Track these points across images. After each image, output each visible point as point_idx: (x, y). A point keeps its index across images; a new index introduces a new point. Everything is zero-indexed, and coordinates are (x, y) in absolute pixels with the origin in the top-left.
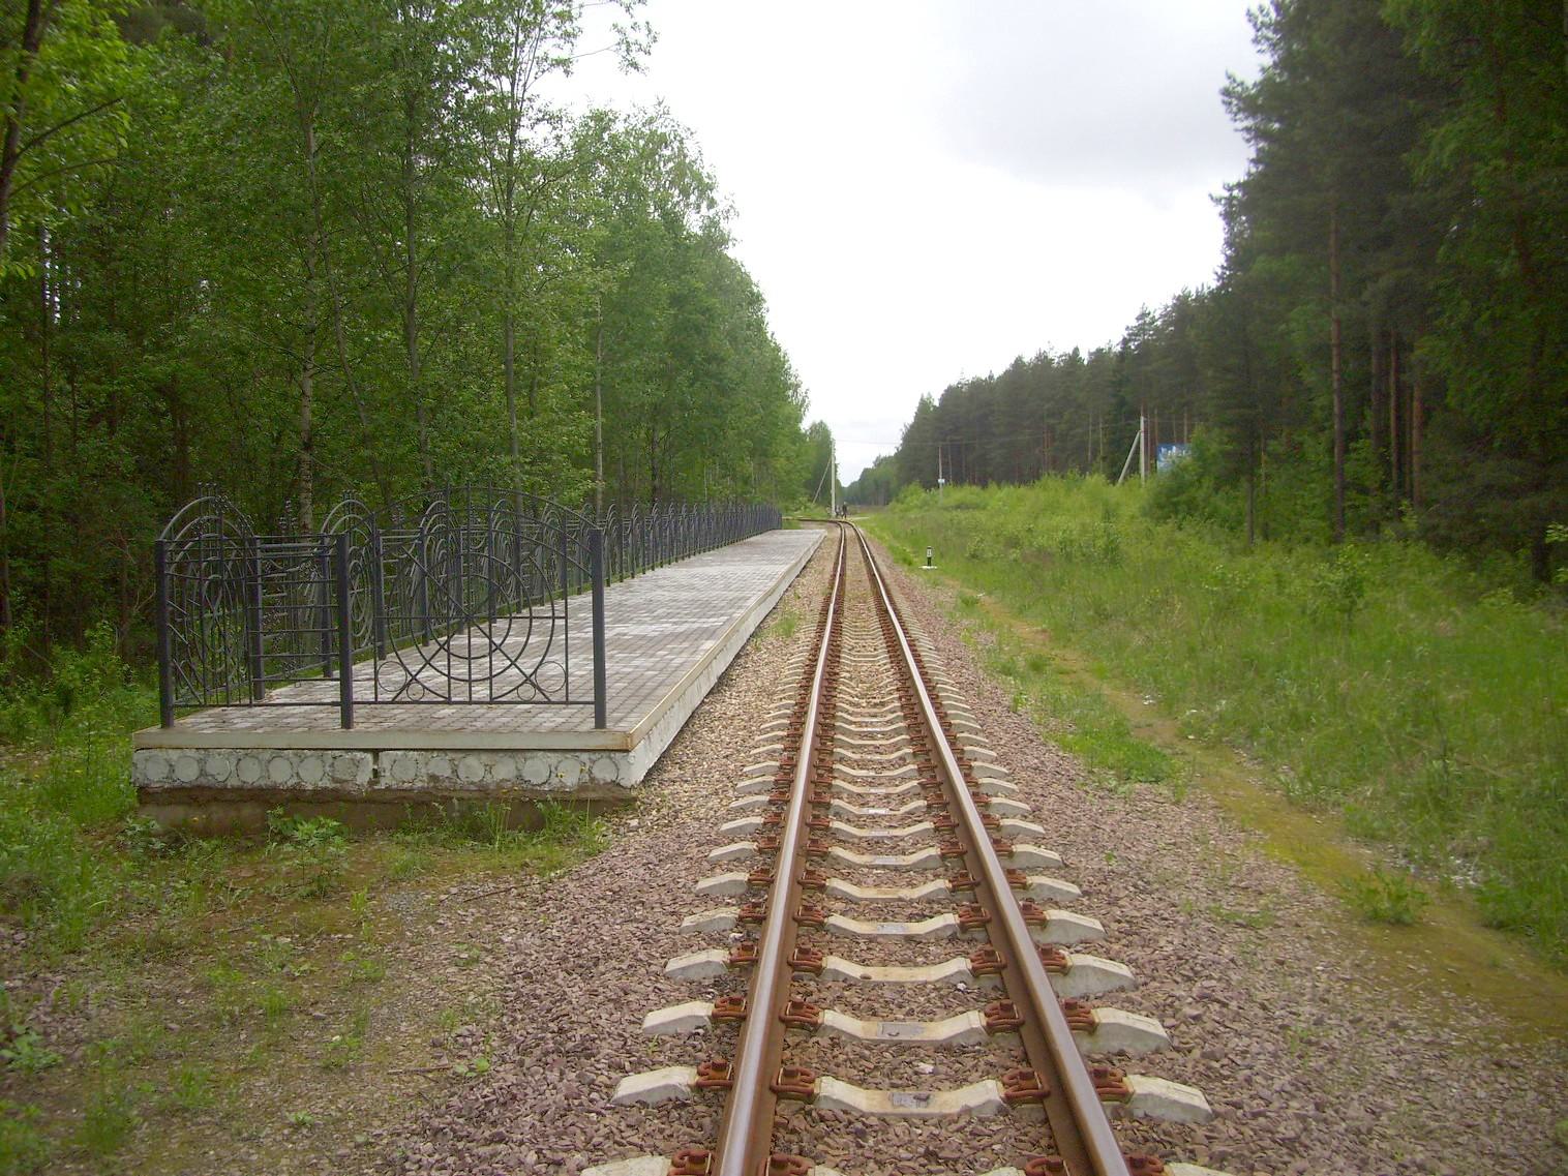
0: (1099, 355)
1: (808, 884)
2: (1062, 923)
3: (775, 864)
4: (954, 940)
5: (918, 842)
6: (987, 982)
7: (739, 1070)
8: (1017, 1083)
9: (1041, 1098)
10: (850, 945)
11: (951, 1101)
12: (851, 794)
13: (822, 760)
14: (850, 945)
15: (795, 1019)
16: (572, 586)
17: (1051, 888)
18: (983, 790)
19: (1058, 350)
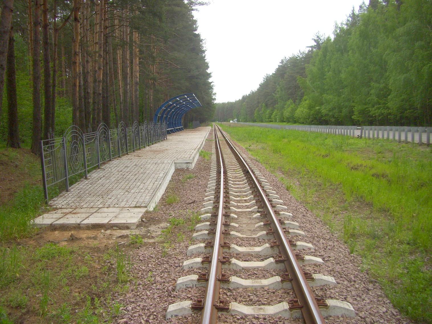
0: (249, 94)
1: (225, 234)
2: (335, 307)
3: (214, 238)
4: (261, 228)
5: (250, 200)
6: (281, 266)
7: (205, 304)
8: (284, 277)
9: (301, 308)
10: (239, 256)
11: (265, 282)
12: (235, 200)
13: (226, 200)
14: (239, 256)
15: (224, 261)
16: (142, 145)
17: (303, 246)
18: (287, 226)
19: (247, 93)
